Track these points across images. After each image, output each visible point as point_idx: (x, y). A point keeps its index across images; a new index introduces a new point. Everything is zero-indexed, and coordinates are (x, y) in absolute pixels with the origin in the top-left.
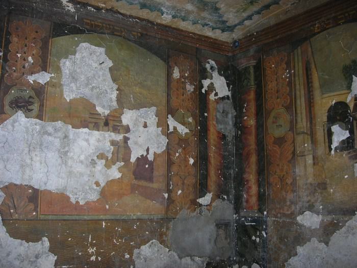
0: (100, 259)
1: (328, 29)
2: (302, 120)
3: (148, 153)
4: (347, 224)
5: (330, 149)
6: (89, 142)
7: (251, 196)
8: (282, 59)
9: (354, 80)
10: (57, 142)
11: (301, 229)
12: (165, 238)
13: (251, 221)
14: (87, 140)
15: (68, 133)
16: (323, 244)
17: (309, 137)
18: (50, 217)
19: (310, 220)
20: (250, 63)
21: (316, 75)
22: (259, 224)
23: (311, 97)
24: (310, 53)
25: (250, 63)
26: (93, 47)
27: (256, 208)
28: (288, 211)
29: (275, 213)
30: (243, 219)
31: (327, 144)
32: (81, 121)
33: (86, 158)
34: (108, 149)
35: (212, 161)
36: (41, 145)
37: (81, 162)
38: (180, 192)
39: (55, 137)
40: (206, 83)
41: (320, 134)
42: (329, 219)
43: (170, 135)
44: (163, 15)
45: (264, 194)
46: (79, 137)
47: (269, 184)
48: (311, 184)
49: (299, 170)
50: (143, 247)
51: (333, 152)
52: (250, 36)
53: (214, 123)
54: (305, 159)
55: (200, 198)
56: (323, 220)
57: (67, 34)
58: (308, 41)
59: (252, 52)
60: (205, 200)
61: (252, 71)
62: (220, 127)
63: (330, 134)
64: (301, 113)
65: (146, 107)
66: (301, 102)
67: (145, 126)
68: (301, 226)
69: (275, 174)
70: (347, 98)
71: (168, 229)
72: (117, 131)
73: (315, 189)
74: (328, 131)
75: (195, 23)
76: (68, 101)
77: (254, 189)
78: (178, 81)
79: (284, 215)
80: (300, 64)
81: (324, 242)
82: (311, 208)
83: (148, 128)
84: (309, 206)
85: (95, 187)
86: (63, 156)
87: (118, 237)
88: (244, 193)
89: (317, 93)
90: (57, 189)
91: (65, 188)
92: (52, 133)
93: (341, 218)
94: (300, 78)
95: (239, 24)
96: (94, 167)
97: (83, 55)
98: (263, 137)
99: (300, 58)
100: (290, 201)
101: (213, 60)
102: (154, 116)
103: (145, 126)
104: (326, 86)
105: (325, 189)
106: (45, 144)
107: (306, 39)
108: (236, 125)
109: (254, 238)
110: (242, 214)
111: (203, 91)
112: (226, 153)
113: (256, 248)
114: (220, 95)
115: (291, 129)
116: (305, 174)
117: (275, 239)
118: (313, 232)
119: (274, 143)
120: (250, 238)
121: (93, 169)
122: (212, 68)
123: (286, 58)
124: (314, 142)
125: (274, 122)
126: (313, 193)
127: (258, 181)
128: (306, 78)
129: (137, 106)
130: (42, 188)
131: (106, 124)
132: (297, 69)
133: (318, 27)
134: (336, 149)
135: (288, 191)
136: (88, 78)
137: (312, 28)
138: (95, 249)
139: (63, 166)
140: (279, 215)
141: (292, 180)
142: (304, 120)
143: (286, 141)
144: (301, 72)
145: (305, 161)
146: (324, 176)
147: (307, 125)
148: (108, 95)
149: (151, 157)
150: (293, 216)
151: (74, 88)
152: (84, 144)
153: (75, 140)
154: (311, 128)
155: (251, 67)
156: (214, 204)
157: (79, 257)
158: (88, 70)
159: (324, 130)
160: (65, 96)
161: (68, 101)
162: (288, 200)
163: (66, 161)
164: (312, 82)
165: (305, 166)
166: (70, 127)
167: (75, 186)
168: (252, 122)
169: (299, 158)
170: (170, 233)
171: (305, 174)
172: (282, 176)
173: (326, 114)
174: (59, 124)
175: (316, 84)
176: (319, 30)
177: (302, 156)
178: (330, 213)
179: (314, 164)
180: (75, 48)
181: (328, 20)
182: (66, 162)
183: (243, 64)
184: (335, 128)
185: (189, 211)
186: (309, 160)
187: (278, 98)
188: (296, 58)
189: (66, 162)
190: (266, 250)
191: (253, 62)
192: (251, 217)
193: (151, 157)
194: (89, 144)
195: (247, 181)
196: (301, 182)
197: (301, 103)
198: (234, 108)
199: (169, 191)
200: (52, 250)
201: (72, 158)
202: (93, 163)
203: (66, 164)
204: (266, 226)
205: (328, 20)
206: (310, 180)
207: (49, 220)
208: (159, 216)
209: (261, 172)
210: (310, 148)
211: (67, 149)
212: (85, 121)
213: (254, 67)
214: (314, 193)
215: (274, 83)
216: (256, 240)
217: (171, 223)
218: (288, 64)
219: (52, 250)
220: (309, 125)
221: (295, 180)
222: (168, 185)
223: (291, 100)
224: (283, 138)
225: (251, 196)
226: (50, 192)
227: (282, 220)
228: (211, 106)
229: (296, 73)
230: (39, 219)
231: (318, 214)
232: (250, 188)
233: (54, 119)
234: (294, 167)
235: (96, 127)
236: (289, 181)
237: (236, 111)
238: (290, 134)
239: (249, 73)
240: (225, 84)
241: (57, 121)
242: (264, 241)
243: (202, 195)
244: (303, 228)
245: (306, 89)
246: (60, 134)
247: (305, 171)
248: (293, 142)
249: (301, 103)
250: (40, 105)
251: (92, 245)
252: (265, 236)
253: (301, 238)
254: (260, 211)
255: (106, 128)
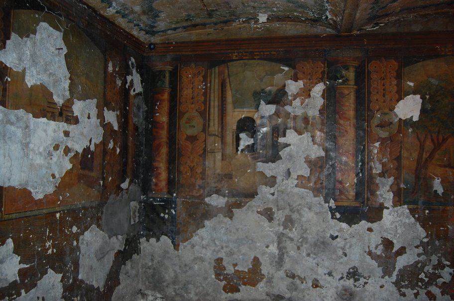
0: (55, 251)
1: (244, 59)
2: (214, 125)
3: (90, 144)
4: (248, 204)
5: (237, 150)
6: (47, 131)
7: (160, 181)
8: (199, 72)
9: (261, 103)
10: (19, 133)
11: (208, 207)
12: (100, 222)
13: (160, 201)
14: (45, 131)
15: (29, 122)
16: (228, 218)
17: (220, 139)
18: (14, 216)
19: (217, 201)
20: (166, 68)
21: (230, 92)
22: (168, 204)
23: (224, 109)
24: (226, 74)
25: (166, 68)
26: (51, 29)
27: (165, 190)
28: (197, 193)
29: (184, 195)
30: (152, 199)
31: (235, 146)
32: (41, 110)
33: (45, 150)
34: (62, 140)
35: (130, 151)
36: (4, 136)
37: (40, 154)
38: (110, 179)
39: (17, 127)
40: (129, 78)
41: (229, 138)
42: (233, 200)
43: (106, 126)
44: (109, 8)
45: (174, 180)
46: (38, 128)
47: (180, 172)
48: (219, 175)
49: (209, 163)
50: (86, 233)
51: (239, 152)
52: (168, 43)
53: (132, 116)
54: (215, 155)
55: (122, 183)
56: (228, 201)
57: (28, 8)
58: (226, 64)
59: (169, 58)
60: (124, 185)
61: (167, 75)
62: (135, 120)
63: (238, 139)
64: (214, 120)
65: (90, 99)
66: (214, 111)
67: (89, 118)
68: (208, 205)
69: (186, 164)
70: (254, 115)
71: (102, 213)
72: (69, 122)
73: (222, 178)
74: (236, 136)
75: (130, 22)
76: (29, 87)
77: (164, 175)
78: (112, 74)
79: (193, 196)
80: (217, 81)
81: (228, 217)
82: (218, 192)
83: (90, 119)
84: (216, 190)
85: (52, 179)
86: (24, 148)
87: (69, 227)
88: (152, 178)
89: (229, 107)
90: (20, 185)
91: (27, 183)
92: (15, 123)
93: (243, 200)
94: (215, 93)
95: (163, 31)
96: (51, 159)
97: (42, 36)
98: (176, 133)
99: (217, 76)
100: (199, 186)
101: (134, 58)
102: (95, 108)
103: (89, 118)
104: (238, 104)
105: (231, 178)
106: (8, 135)
107: (224, 62)
108: (146, 119)
109: (162, 215)
110: (150, 195)
111: (127, 87)
112: (138, 143)
113: (164, 223)
114: (137, 92)
115: (204, 130)
116: (214, 167)
117: (184, 215)
118: (220, 210)
119: (186, 139)
120: (158, 215)
121: (50, 161)
122: (132, 64)
123: (204, 72)
124: (223, 142)
125: (187, 123)
126: (220, 181)
127: (168, 168)
128: (220, 93)
129: (84, 97)
130: (6, 185)
131: (61, 114)
132: (213, 83)
133: (236, 56)
134: (242, 150)
135: (197, 179)
136: (46, 62)
137: (230, 55)
138: (51, 242)
139: (25, 158)
140: (188, 197)
141: (201, 170)
142: (216, 126)
143: (198, 140)
144: (217, 87)
145: (215, 157)
146: (230, 169)
147: (218, 129)
148: (62, 83)
149: (92, 148)
150: (201, 198)
151: (35, 72)
152: (43, 134)
153: (35, 130)
154: (222, 132)
155: (167, 71)
156: (130, 188)
157: (38, 252)
158: (46, 54)
159: (233, 136)
160: (26, 81)
161: (29, 87)
162: (197, 185)
163: (27, 153)
164: (225, 97)
165: (215, 161)
166: (31, 115)
167: (34, 180)
168: (164, 119)
169: (209, 154)
170: (103, 217)
171: (214, 167)
172: (192, 166)
173: (236, 124)
174: (21, 112)
175: (229, 99)
176: (237, 58)
177: (213, 152)
178: (233, 196)
179: (222, 160)
180: (36, 27)
181: (247, 52)
182: (27, 155)
183: (158, 67)
184: (242, 135)
185: (115, 195)
186: (219, 156)
187: (192, 103)
188: (213, 75)
189: (27, 155)
190: (174, 224)
191: (170, 68)
192: (160, 198)
193: (92, 148)
194: (47, 135)
195: (157, 168)
196: (209, 172)
197: (215, 112)
198: (145, 104)
199: (103, 179)
200: (16, 251)
201: (33, 150)
202: (50, 155)
203: (27, 156)
204: (176, 205)
205: (247, 52)
206: (218, 171)
207: (12, 219)
208: (97, 202)
209: (173, 160)
210: (220, 148)
211: (28, 140)
212: (44, 110)
213: (170, 72)
214: (221, 181)
215: (190, 91)
216: (164, 216)
217: (104, 208)
218: (205, 77)
219: (16, 251)
220: (220, 130)
221: (204, 170)
222: (103, 173)
223: (205, 108)
224: (196, 136)
225: (160, 181)
226: (14, 188)
227: (191, 200)
228: (131, 100)
229: (212, 87)
230: (3, 219)
231: (224, 196)
232: (160, 174)
233: (17, 107)
234: (204, 160)
235: (53, 118)
236: (199, 170)
237: (147, 107)
238: (202, 135)
239: (164, 77)
240: (140, 81)
241: (19, 109)
242: (173, 218)
243: (123, 182)
244: (210, 206)
245: (220, 102)
246: (22, 124)
247: (215, 164)
248: (205, 141)
249: (215, 112)
250: (3, 89)
251: (49, 238)
252: (174, 213)
253: (208, 214)
254: (170, 193)
255: (61, 118)
